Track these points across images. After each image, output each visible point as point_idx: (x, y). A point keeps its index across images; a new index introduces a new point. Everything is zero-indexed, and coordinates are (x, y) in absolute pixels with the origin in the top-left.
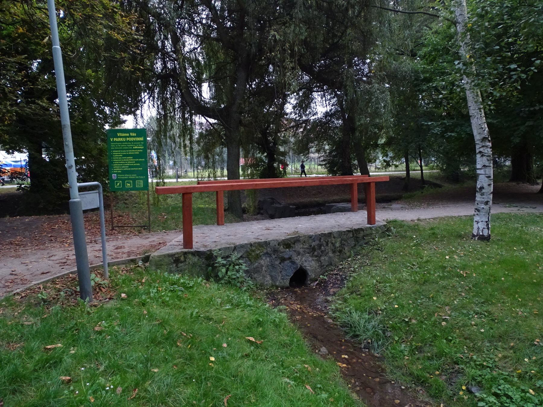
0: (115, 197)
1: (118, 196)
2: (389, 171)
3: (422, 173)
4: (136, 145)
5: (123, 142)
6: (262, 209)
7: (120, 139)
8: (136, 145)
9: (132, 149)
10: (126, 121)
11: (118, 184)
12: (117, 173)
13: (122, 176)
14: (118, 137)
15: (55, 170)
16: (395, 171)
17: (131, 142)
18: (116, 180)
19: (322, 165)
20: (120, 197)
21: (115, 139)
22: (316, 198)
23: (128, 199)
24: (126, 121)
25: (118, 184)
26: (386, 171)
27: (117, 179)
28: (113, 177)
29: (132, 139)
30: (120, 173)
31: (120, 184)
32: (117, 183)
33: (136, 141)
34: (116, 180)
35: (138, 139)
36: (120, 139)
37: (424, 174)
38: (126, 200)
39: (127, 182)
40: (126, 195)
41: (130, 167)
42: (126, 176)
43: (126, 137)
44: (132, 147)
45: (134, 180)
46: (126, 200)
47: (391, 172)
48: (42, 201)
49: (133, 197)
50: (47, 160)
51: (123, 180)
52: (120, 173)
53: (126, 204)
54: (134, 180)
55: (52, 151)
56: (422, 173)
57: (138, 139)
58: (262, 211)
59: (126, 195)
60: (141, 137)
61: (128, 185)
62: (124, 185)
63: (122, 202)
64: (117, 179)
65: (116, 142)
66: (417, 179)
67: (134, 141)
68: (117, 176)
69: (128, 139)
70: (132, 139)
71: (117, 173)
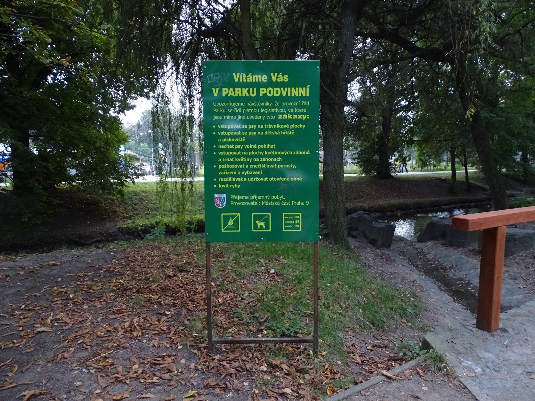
0: (122, 201)
1: (125, 199)
2: (427, 171)
3: (467, 172)
4: (287, 108)
5: (250, 99)
6: (356, 229)
7: (240, 92)
8: (287, 108)
9: (276, 121)
10: (134, 106)
11: (231, 222)
12: (228, 192)
13: (239, 200)
14: (233, 85)
15: (45, 167)
16: (433, 170)
17: (273, 99)
18: (225, 210)
19: (355, 163)
20: (128, 201)
21: (225, 91)
22: (358, 202)
23: (138, 203)
24: (134, 106)
25: (231, 222)
26: (422, 171)
27: (229, 208)
28: (217, 202)
29: (276, 92)
30: (236, 192)
31: (236, 222)
32: (227, 219)
33: (287, 99)
34: (225, 210)
35: (295, 92)
36: (240, 92)
37: (469, 174)
38: (136, 205)
39: (257, 218)
40: (136, 199)
41: (267, 172)
42: (254, 201)
43: (258, 85)
44: (276, 114)
45: (277, 212)
46: (136, 205)
47: (429, 173)
48: (27, 211)
49: (144, 201)
50: (36, 153)
51: (246, 212)
52: (236, 192)
53: (136, 209)
54: (277, 212)
55: (41, 141)
56: (467, 172)
57: (295, 92)
58: (354, 233)
59: (136, 199)
60: (303, 86)
61: (259, 224)
62: (246, 223)
63: (131, 207)
64: (229, 208)
65: (227, 99)
66: (462, 181)
67: (281, 99)
68: (228, 200)
69: (263, 91)
70: (276, 92)
71: (228, 192)
